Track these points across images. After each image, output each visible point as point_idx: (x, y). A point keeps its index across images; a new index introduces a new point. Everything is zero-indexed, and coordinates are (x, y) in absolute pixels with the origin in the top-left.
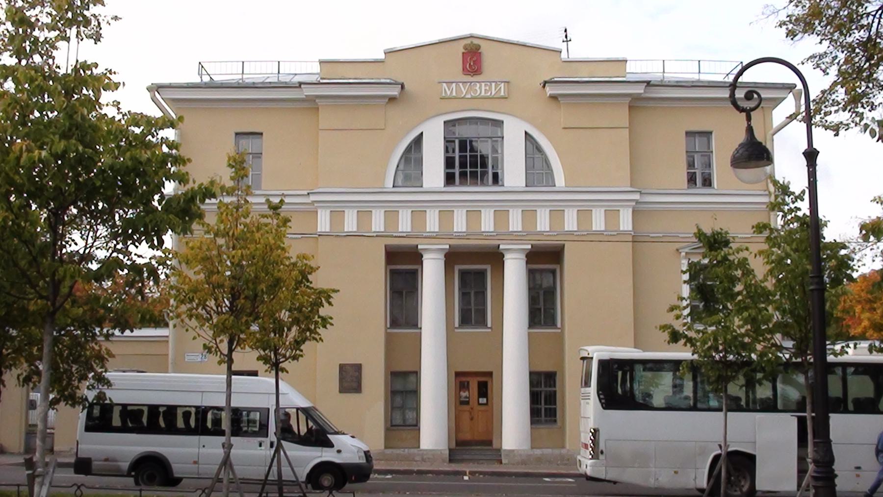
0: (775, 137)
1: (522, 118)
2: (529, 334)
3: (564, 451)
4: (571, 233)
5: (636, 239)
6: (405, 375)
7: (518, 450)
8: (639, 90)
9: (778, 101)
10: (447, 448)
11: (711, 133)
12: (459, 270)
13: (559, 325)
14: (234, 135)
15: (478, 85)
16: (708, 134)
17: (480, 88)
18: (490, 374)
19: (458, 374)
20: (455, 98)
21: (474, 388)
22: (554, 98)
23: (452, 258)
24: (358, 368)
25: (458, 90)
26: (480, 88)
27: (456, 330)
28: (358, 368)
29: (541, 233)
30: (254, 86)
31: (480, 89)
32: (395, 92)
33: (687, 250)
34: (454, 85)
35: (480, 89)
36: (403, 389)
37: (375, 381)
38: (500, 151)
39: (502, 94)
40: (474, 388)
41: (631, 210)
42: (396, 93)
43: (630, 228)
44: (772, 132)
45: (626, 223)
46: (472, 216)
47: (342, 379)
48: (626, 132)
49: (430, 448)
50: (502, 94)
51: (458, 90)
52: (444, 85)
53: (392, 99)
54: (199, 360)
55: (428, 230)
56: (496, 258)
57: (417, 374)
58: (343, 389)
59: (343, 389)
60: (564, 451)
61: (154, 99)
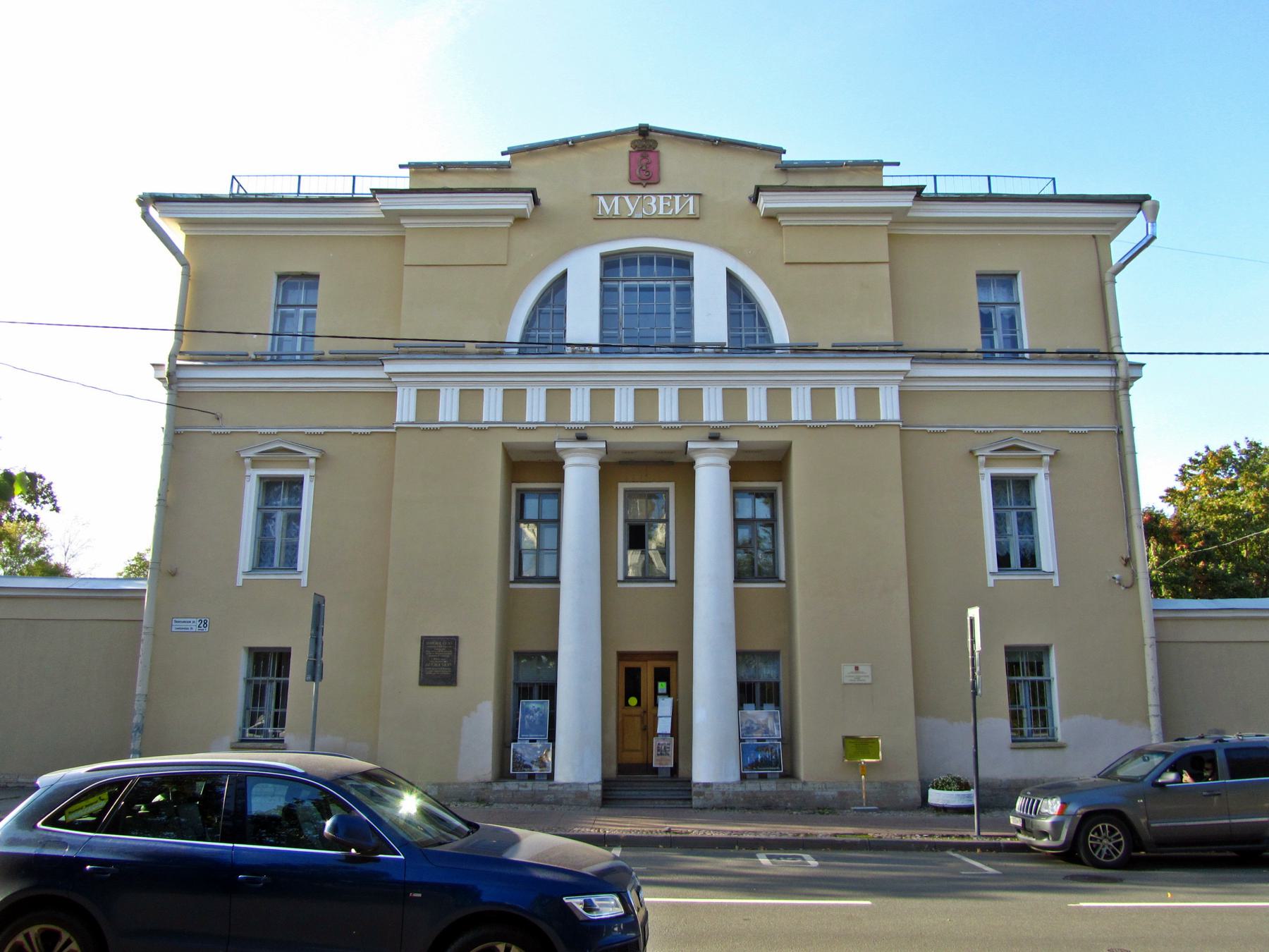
0: (1117, 278)
1: (726, 249)
2: (736, 590)
3: (796, 787)
4: (801, 425)
5: (905, 429)
6: (533, 656)
7: (718, 785)
8: (906, 201)
9: (1120, 225)
10: (598, 778)
11: (1015, 275)
12: (626, 491)
13: (782, 576)
14: (275, 279)
15: (654, 199)
16: (1007, 280)
17: (657, 203)
18: (673, 656)
19: (622, 656)
20: (618, 218)
21: (645, 677)
22: (771, 217)
23: (615, 468)
24: (452, 643)
25: (623, 206)
26: (657, 203)
27: (620, 585)
28: (452, 643)
29: (754, 426)
30: (308, 200)
31: (657, 205)
32: (522, 203)
33: (987, 452)
34: (616, 198)
35: (657, 205)
36: (530, 680)
37: (480, 666)
38: (667, 256)
39: (691, 212)
40: (645, 677)
41: (896, 388)
42: (524, 207)
43: (897, 417)
44: (1110, 270)
45: (889, 408)
46: (646, 397)
47: (425, 661)
48: (884, 271)
49: (571, 779)
50: (691, 212)
51: (623, 206)
52: (601, 198)
53: (520, 219)
54: (195, 629)
55: (572, 420)
56: (680, 468)
57: (553, 656)
58: (427, 679)
59: (427, 679)
60: (796, 787)
61: (146, 216)
